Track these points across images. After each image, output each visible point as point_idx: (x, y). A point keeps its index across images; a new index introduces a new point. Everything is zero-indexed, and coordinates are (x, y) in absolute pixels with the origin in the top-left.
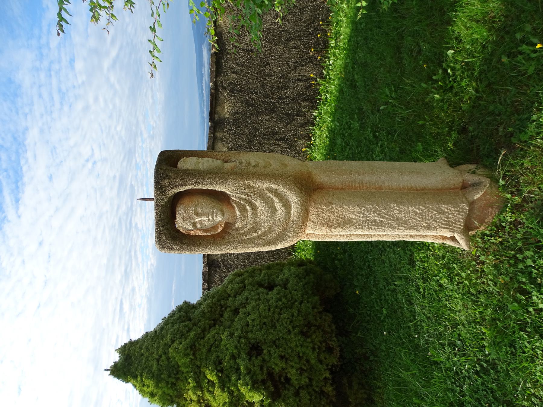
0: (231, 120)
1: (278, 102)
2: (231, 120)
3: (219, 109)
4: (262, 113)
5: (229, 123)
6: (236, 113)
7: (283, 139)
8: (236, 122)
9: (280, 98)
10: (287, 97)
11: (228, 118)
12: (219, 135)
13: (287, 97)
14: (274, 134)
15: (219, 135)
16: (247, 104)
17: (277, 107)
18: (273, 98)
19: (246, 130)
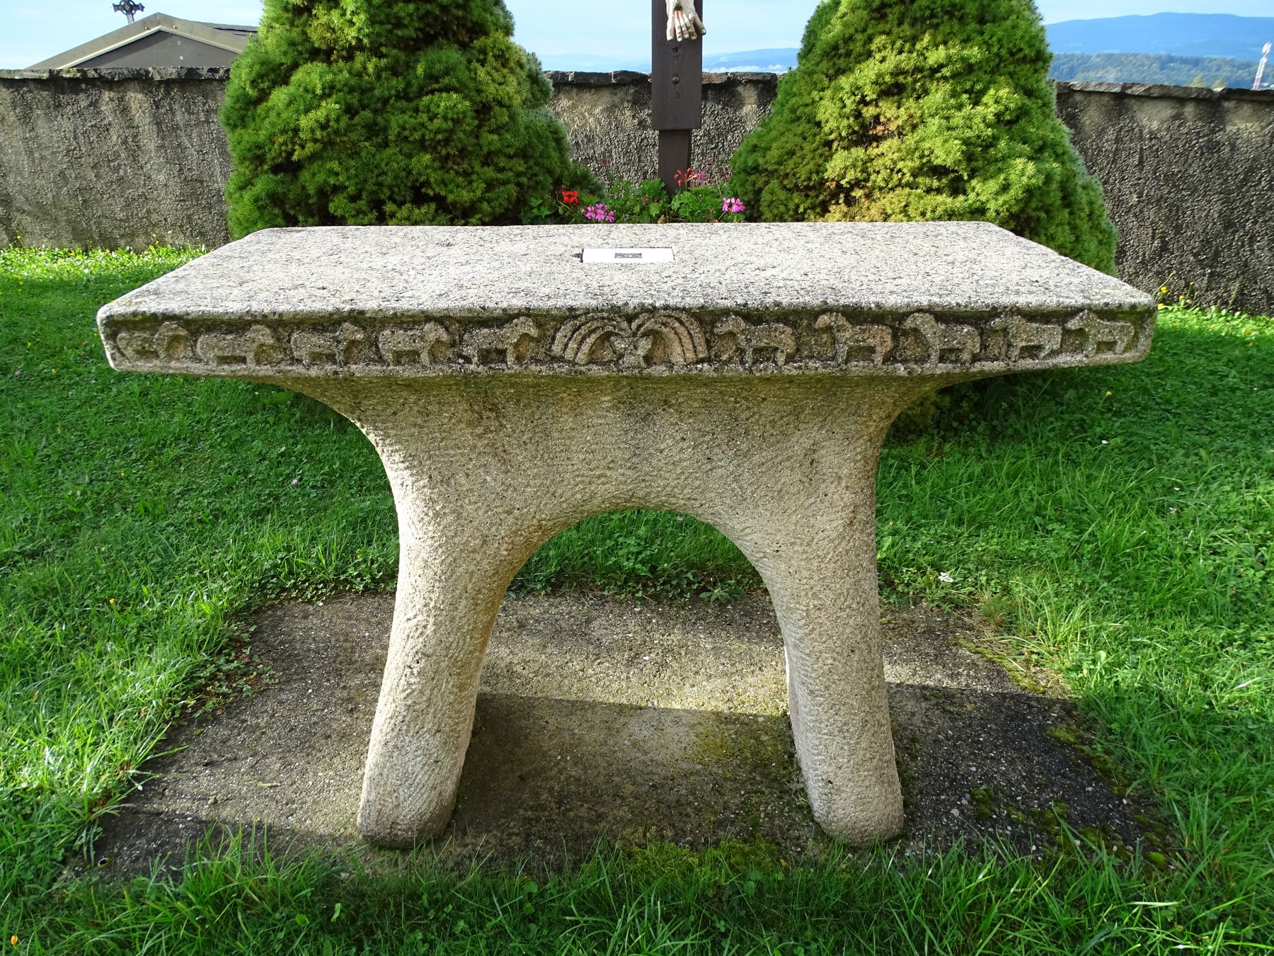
0: (1219, 136)
1: (1246, 234)
2: (1219, 136)
3: (1247, 109)
4: (1227, 201)
5: (1213, 131)
6: (1233, 147)
7: (1164, 248)
8: (1213, 147)
9: (1252, 240)
10: (1252, 251)
11: (1223, 129)
12: (1189, 110)
13: (1252, 251)
14: (1178, 229)
15: (1189, 110)
16: (1251, 171)
17: (1234, 233)
18: (1255, 223)
19: (1195, 170)
